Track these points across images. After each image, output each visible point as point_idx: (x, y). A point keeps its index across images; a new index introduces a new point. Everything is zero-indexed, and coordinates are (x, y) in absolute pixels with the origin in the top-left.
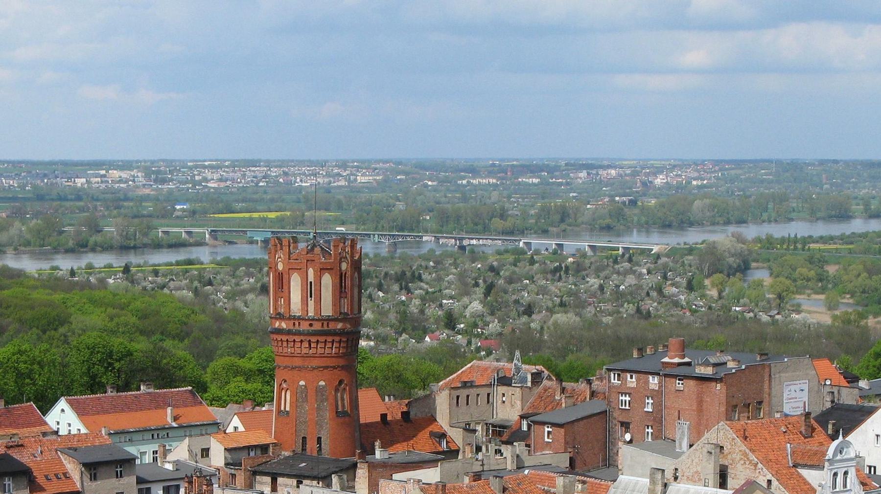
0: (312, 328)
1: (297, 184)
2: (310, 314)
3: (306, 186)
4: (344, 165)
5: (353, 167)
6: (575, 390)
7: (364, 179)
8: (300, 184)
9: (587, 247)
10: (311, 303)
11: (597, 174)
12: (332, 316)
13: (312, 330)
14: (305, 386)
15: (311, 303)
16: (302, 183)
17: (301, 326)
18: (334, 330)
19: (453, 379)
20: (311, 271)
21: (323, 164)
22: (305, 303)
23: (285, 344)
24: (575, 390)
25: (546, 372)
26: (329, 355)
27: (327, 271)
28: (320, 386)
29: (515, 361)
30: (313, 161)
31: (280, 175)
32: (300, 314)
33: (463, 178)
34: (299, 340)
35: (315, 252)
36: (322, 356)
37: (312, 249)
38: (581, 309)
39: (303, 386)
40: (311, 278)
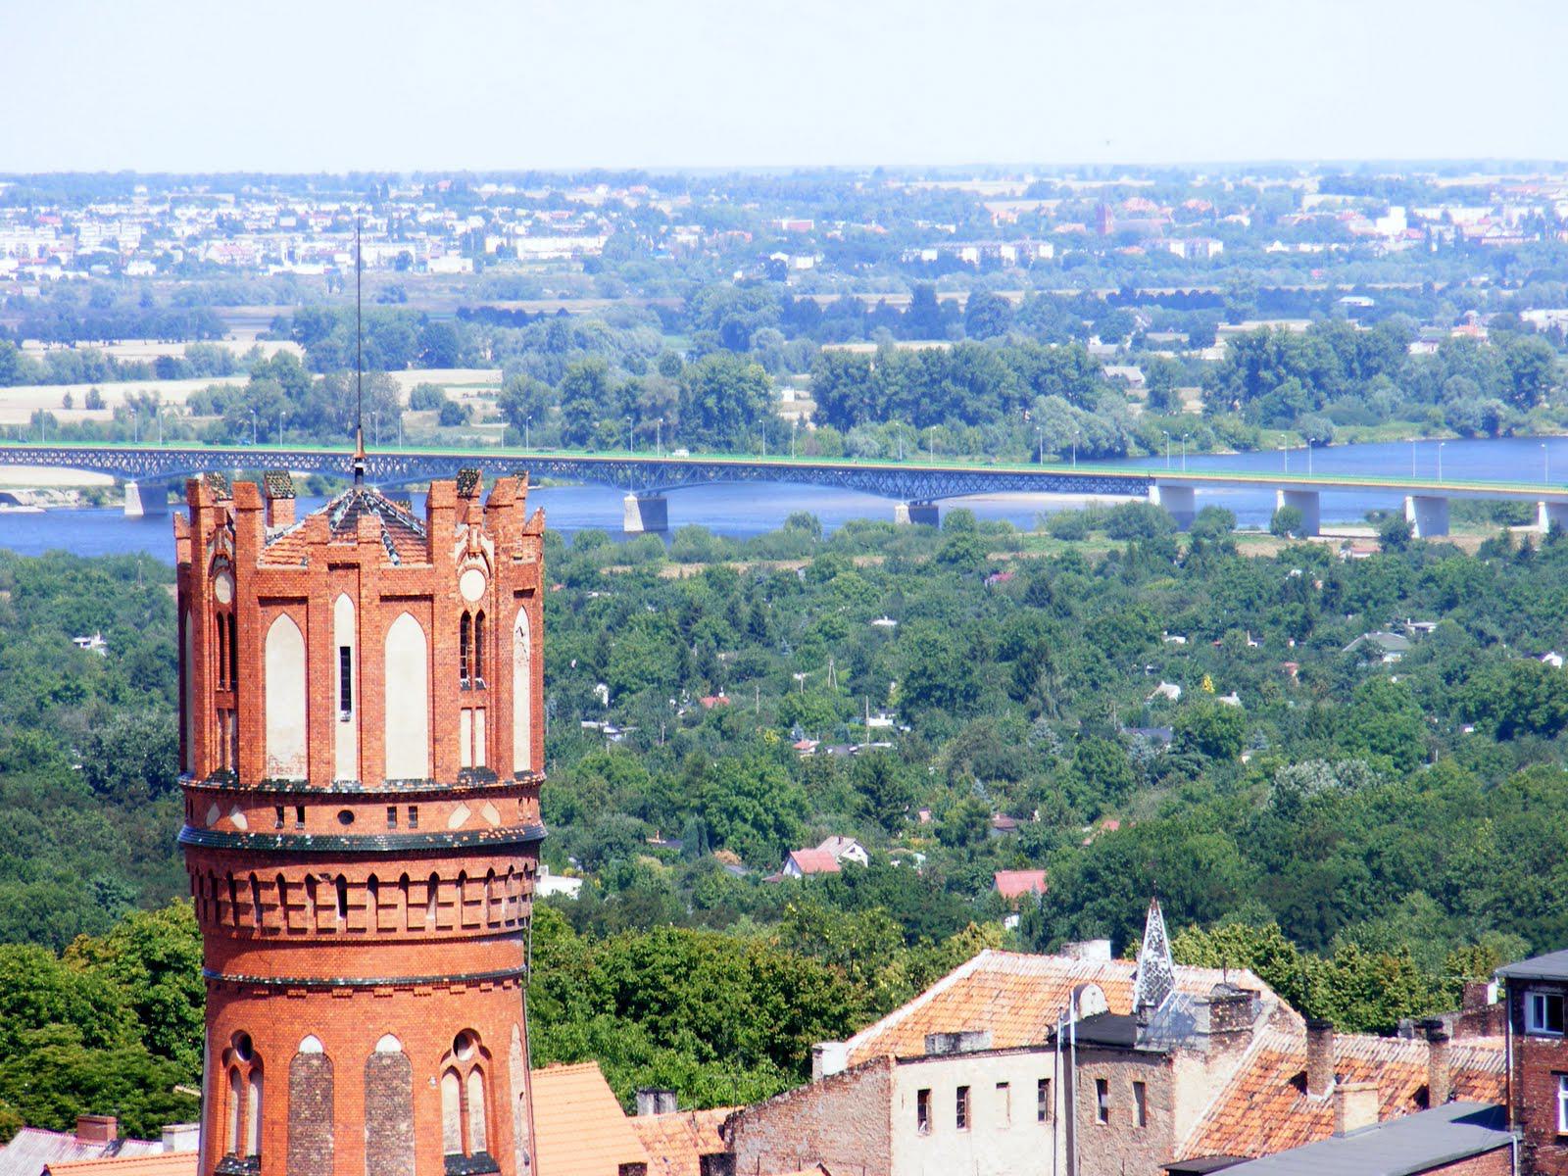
0: (353, 830)
1: (274, 269)
2: (340, 777)
3: (308, 276)
4: (457, 193)
5: (492, 201)
6: (1380, 1065)
7: (546, 247)
8: (288, 266)
9: (1410, 502)
10: (345, 734)
11: (1446, 218)
12: (429, 781)
13: (351, 839)
14: (325, 1058)
15: (345, 734)
16: (295, 262)
17: (307, 824)
18: (433, 835)
19: (902, 1027)
20: (344, 610)
21: (375, 190)
22: (316, 725)
23: (419, 894)
24: (1380, 1065)
25: (1267, 994)
26: (470, 933)
27: (406, 605)
28: (380, 1057)
29: (1147, 953)
30: (336, 178)
31: (207, 234)
32: (303, 777)
33: (927, 239)
34: (424, 876)
35: (362, 533)
36: (472, 936)
37: (350, 523)
38: (1028, 241)
39: (316, 1056)
40: (344, 632)
